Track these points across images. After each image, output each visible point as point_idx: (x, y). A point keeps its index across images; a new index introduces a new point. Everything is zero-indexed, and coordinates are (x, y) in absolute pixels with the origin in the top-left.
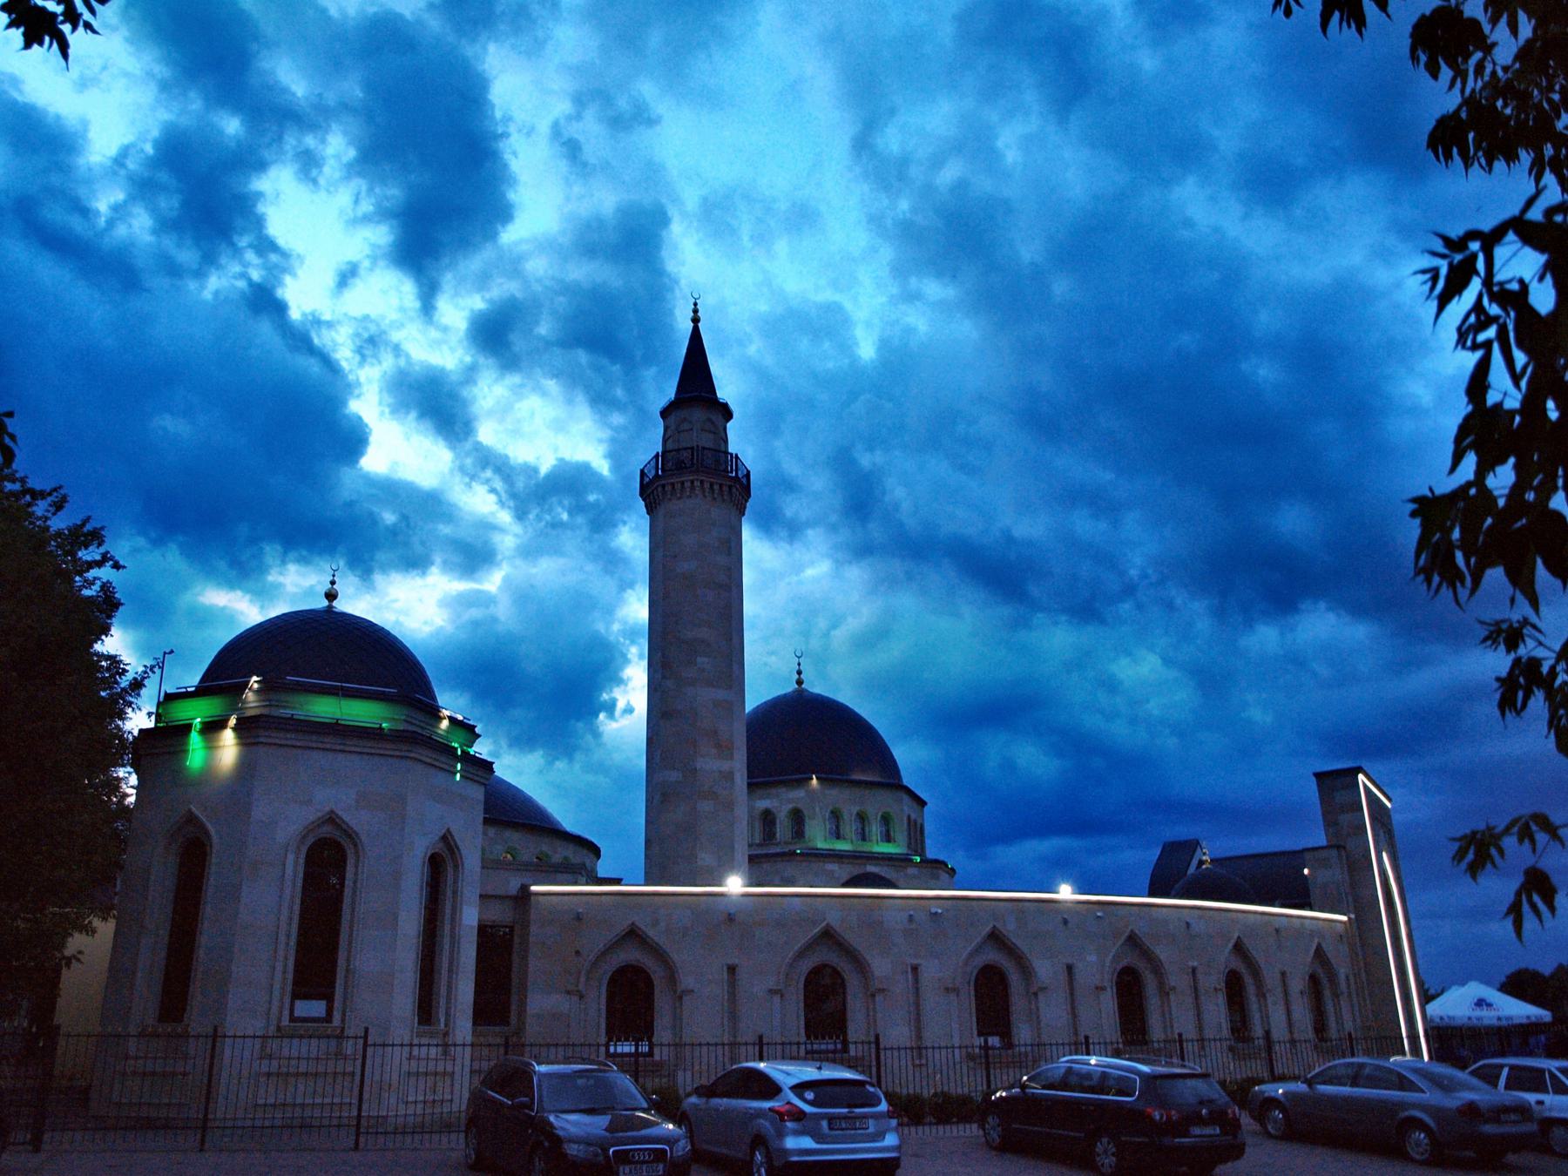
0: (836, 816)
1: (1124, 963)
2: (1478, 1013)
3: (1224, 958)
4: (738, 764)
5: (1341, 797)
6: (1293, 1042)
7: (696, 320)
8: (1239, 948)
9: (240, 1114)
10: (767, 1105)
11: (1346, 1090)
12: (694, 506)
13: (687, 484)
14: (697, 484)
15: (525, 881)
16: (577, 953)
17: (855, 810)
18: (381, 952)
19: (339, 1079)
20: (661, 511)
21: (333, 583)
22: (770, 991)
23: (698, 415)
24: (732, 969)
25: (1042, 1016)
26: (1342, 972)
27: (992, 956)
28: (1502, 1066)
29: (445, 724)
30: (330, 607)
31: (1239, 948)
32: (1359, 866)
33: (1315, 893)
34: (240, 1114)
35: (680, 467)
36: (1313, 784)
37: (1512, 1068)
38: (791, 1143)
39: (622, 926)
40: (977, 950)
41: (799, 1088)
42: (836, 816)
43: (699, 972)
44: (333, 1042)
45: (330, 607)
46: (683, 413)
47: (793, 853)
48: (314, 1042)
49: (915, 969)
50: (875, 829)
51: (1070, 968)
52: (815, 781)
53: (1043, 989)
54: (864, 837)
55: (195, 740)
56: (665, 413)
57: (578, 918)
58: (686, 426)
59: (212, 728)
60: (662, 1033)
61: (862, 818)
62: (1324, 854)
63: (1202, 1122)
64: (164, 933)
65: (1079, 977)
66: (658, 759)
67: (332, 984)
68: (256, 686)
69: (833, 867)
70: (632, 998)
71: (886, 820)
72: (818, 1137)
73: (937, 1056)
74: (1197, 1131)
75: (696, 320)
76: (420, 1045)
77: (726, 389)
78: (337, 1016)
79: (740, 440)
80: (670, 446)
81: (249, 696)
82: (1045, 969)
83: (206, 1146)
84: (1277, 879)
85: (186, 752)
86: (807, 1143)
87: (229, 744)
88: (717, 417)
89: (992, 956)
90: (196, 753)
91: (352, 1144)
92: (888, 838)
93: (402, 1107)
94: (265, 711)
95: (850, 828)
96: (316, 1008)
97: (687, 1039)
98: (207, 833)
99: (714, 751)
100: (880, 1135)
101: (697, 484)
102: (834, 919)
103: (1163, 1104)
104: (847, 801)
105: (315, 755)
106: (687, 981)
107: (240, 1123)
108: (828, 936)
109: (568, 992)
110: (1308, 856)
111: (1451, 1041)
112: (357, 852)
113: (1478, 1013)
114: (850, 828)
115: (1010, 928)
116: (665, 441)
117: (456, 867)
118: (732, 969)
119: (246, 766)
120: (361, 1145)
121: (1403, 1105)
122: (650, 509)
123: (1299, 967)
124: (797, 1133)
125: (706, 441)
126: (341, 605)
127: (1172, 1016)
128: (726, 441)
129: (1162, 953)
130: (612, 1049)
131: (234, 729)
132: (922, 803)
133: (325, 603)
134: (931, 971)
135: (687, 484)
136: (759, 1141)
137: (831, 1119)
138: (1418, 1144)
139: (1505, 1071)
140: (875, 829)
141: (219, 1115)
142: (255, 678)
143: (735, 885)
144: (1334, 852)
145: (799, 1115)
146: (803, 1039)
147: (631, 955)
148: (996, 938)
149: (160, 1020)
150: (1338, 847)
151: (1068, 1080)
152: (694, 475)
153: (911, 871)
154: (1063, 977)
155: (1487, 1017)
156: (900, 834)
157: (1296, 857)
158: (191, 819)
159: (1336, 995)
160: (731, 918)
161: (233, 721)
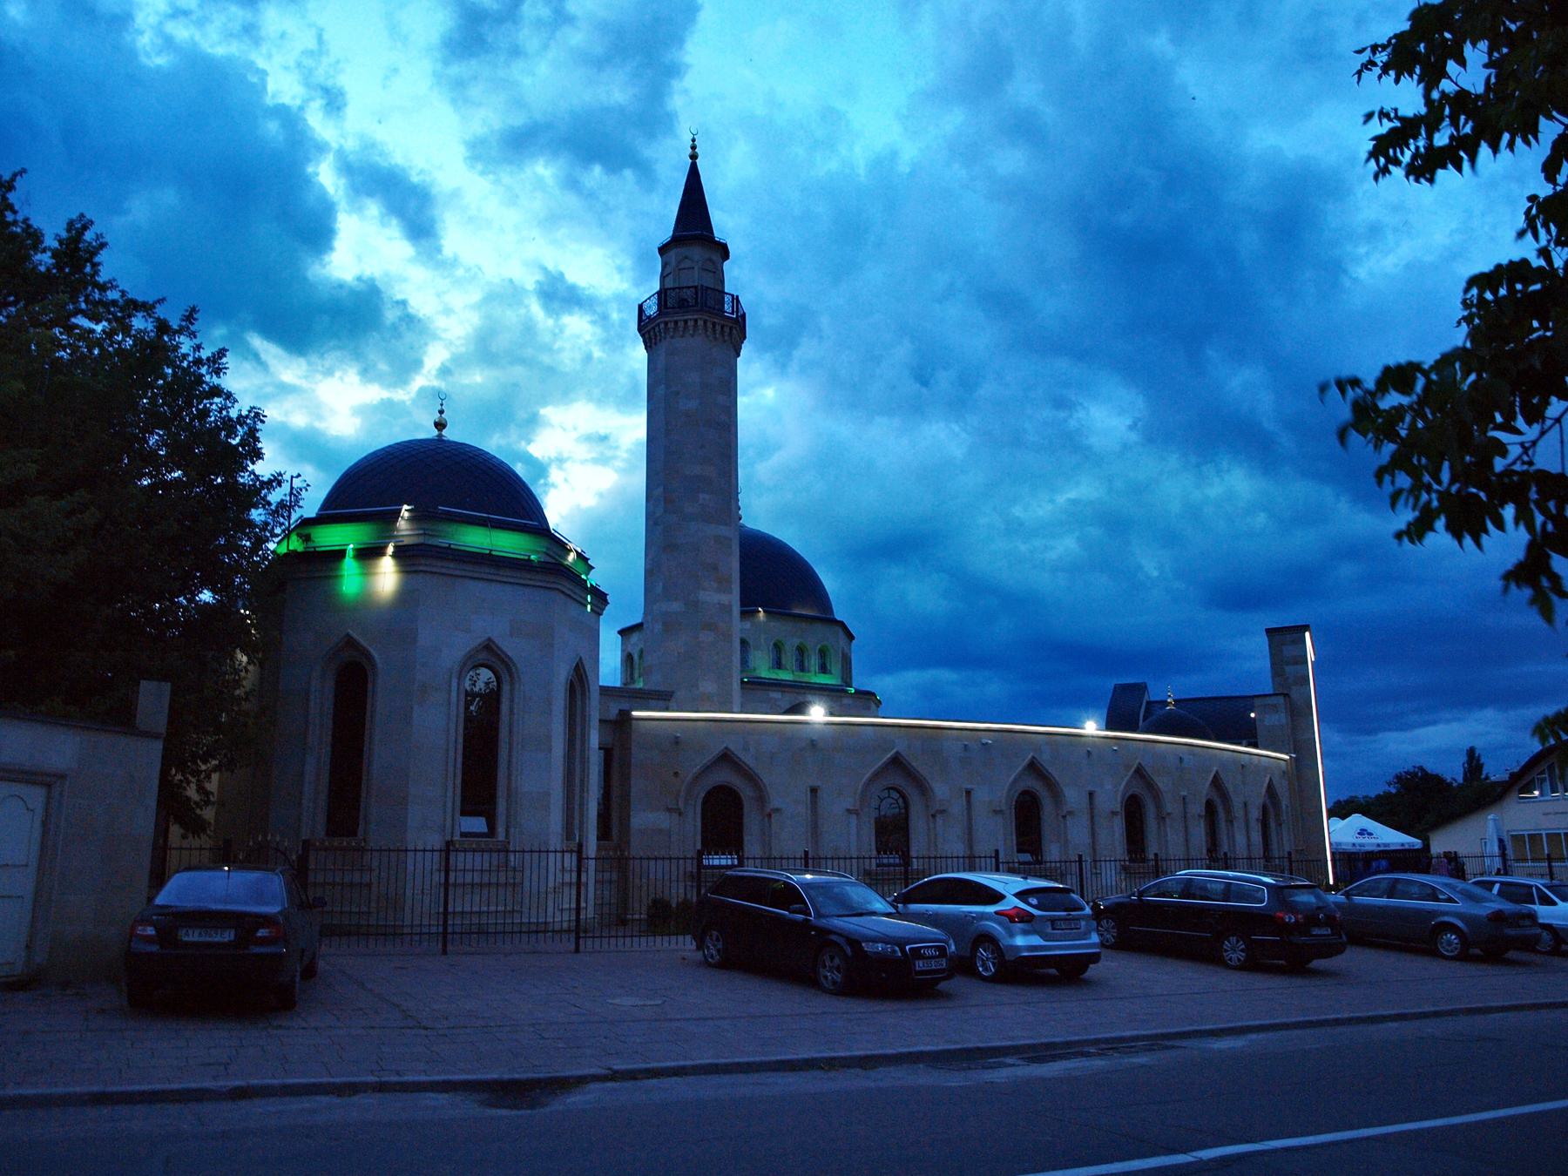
0: (778, 648)
1: (1021, 787)
2: (1361, 840)
3: (1204, 789)
4: (734, 598)
5: (1289, 651)
6: (1250, 858)
7: (694, 157)
8: (1217, 783)
9: (425, 922)
10: (991, 909)
11: (1384, 900)
12: (692, 345)
13: (691, 323)
14: (700, 323)
15: (625, 706)
16: (676, 774)
17: (796, 642)
18: (538, 775)
19: (477, 891)
20: (663, 347)
21: (441, 412)
22: (848, 811)
23: (697, 253)
24: (814, 791)
25: (1165, 839)
26: (1284, 802)
27: (1138, 789)
28: (1493, 883)
29: (571, 557)
30: (440, 436)
31: (1217, 783)
32: (1299, 713)
33: (1261, 732)
34: (425, 922)
35: (683, 305)
36: (1263, 641)
37: (1502, 883)
38: (1020, 941)
39: (717, 750)
40: (1020, 776)
41: (1021, 895)
42: (778, 648)
43: (786, 794)
44: (502, 855)
45: (440, 436)
46: (684, 251)
47: (1124, 711)
48: (469, 855)
49: (968, 793)
50: (814, 662)
51: (1091, 794)
52: (762, 614)
53: (1070, 813)
54: (802, 668)
55: (349, 566)
56: (663, 250)
57: (677, 741)
58: (687, 264)
59: (368, 554)
60: (752, 847)
61: (801, 651)
62: (1269, 701)
63: (1318, 924)
64: (326, 750)
65: (1098, 800)
66: (659, 589)
67: (492, 799)
68: (406, 515)
69: (775, 695)
70: (724, 816)
71: (823, 654)
72: (1045, 937)
73: (410, 861)
74: (1316, 931)
75: (694, 157)
76: (181, 848)
77: (723, 223)
78: (501, 830)
79: (739, 277)
80: (670, 284)
81: (402, 525)
82: (1073, 797)
83: (450, 947)
84: (1225, 717)
85: (338, 577)
86: (1036, 940)
87: (387, 576)
88: (716, 257)
89: (897, 780)
90: (350, 578)
91: (573, 947)
92: (824, 669)
93: (558, 914)
94: (420, 540)
95: (789, 658)
96: (478, 824)
97: (775, 854)
98: (369, 657)
99: (715, 585)
100: (1086, 935)
101: (700, 323)
102: (900, 747)
103: (1292, 908)
104: (790, 635)
105: (472, 585)
106: (775, 802)
107: (425, 930)
108: (897, 762)
109: (669, 810)
110: (1257, 702)
111: (1354, 863)
112: (511, 675)
113: (1361, 840)
114: (789, 658)
115: (1045, 759)
116: (663, 278)
117: (583, 694)
118: (814, 791)
119: (405, 595)
120: (582, 948)
121: (1433, 914)
122: (649, 346)
123: (1258, 797)
124: (1025, 933)
125: (708, 281)
126: (450, 434)
127: (1068, 836)
128: (722, 282)
129: (1162, 783)
130: (705, 862)
131: (394, 556)
132: (851, 637)
133: (436, 432)
134: (981, 795)
135: (691, 323)
136: (987, 939)
137: (1053, 921)
138: (1449, 943)
139: (1497, 886)
140: (814, 662)
141: (407, 922)
142: (406, 507)
143: (1091, 728)
144: (1281, 700)
145: (1025, 918)
146: (874, 853)
147: (724, 776)
148: (1034, 767)
149: (327, 834)
150: (1286, 695)
151: (1188, 889)
152: (692, 315)
153: (845, 701)
154: (1086, 800)
155: (1368, 843)
156: (836, 668)
157: (1248, 701)
158: (350, 643)
159: (1161, 819)
160: (813, 744)
161: (390, 549)
